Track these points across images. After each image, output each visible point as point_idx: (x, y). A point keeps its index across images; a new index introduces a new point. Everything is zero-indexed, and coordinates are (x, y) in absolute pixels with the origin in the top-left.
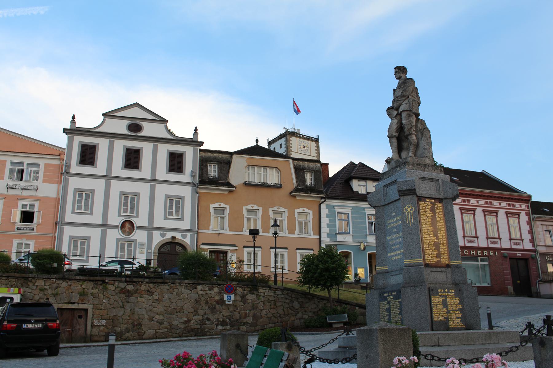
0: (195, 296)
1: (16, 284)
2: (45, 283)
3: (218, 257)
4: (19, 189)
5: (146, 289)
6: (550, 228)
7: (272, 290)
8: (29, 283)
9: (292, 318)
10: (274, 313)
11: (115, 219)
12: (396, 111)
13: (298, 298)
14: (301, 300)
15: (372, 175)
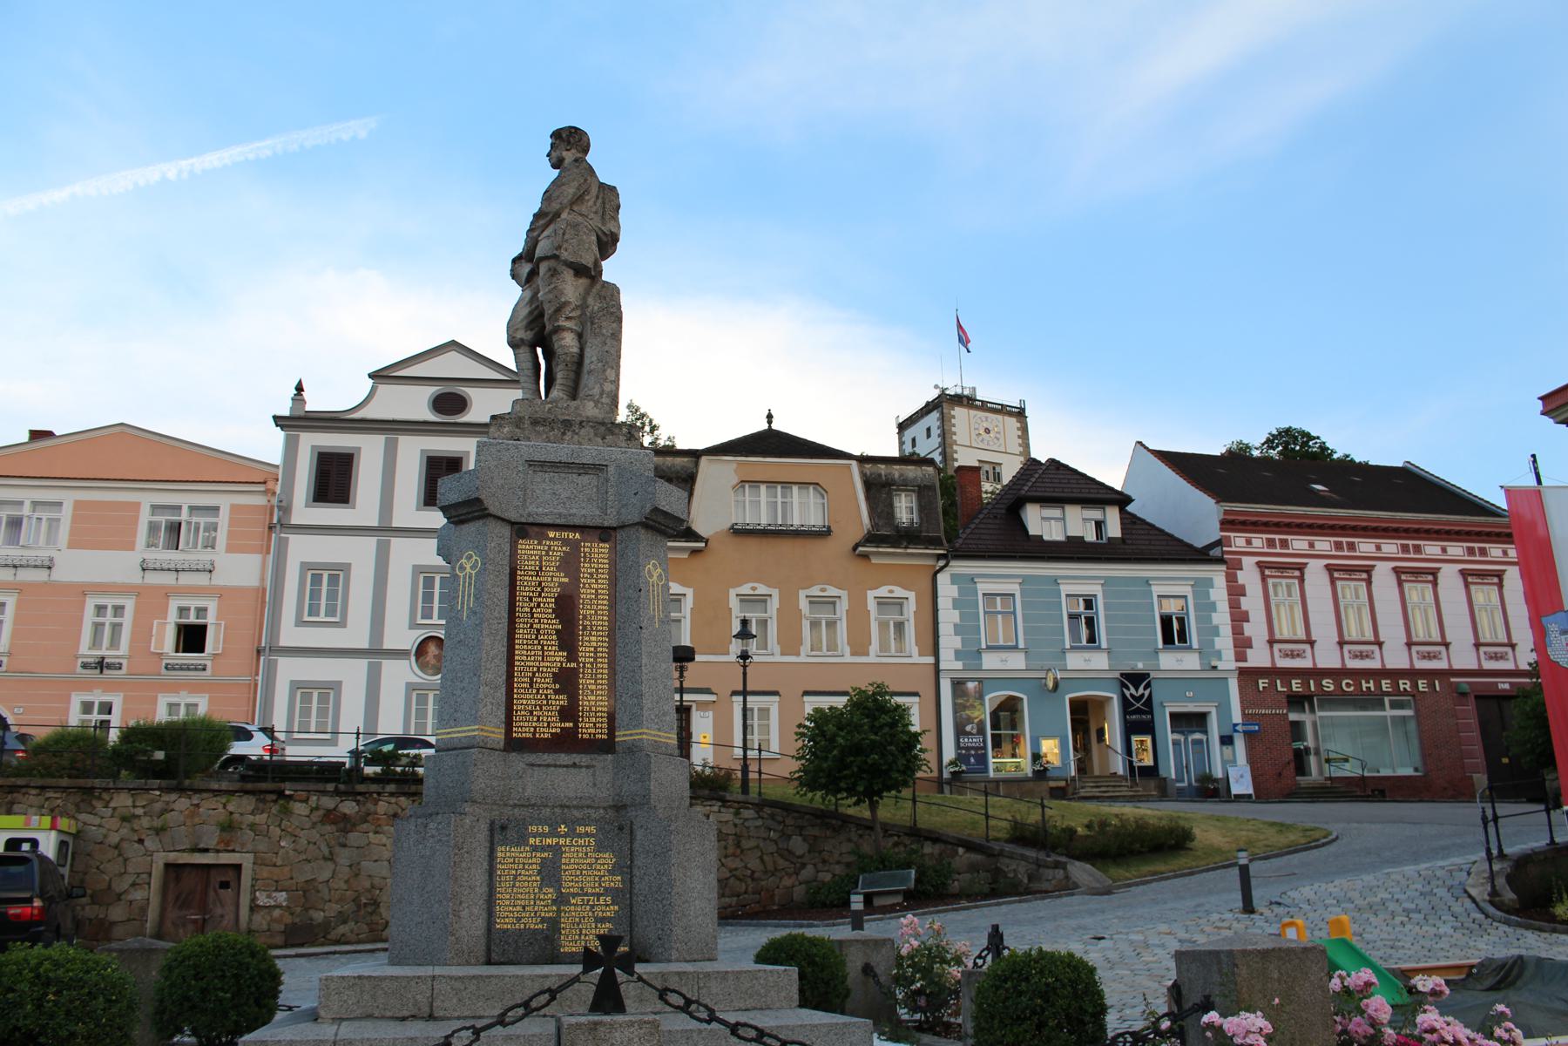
1: (65, 805)
2: (134, 802)
4: (169, 570)
5: (391, 812)
7: (730, 807)
8: (94, 802)
9: (787, 882)
10: (736, 869)
13: (801, 828)
14: (816, 832)
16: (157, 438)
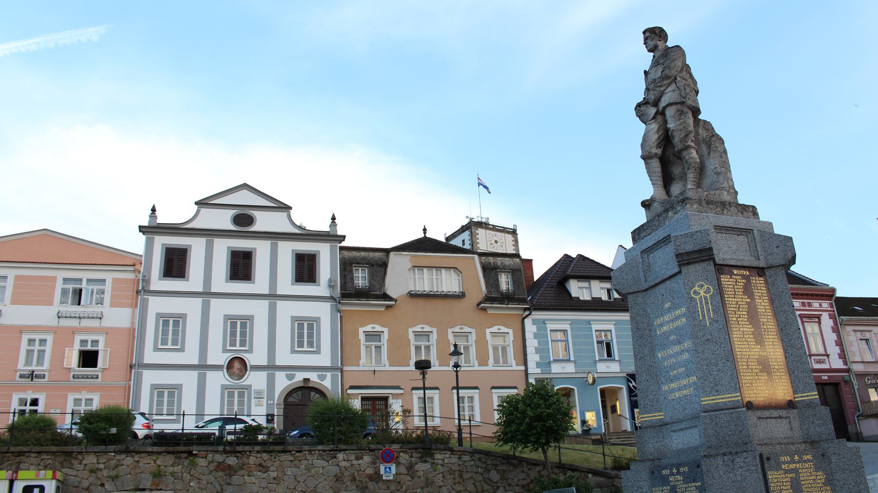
0: (334, 470)
2: (98, 460)
3: (374, 406)
4: (75, 317)
5: (258, 463)
6: (868, 335)
7: (456, 454)
8: (73, 461)
11: (218, 356)
12: (653, 108)
13: (496, 465)
14: (504, 467)
15: (597, 272)
16: (67, 238)
